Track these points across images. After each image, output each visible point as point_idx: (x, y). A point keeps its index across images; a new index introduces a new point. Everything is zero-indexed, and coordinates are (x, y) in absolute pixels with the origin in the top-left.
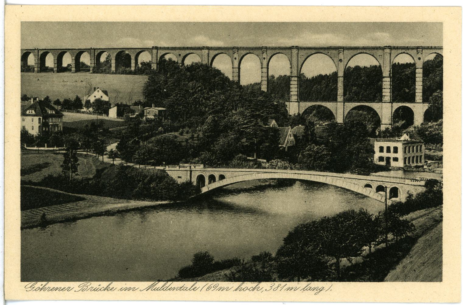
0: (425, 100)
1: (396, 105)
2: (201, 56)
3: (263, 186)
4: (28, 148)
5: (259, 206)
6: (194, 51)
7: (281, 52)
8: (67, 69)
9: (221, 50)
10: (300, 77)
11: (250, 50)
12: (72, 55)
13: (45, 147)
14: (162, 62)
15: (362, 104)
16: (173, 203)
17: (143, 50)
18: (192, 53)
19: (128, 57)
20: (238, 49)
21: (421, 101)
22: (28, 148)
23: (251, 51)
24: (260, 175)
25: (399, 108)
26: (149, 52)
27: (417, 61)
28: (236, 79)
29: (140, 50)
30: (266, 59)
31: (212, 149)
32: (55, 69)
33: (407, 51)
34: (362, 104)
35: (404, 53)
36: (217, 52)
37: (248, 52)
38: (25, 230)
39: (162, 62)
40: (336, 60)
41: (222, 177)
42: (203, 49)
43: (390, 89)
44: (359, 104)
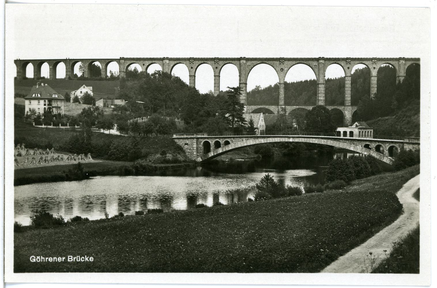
0: (353, 104)
2: (163, 65)
4: (35, 126)
6: (156, 62)
9: (179, 61)
10: (286, 84)
11: (204, 61)
13: (67, 126)
15: (262, 107)
18: (154, 63)
21: (350, 104)
22: (35, 126)
23: (205, 62)
26: (117, 62)
28: (192, 85)
29: (109, 61)
30: (144, 63)
31: (249, 125)
34: (262, 107)
38: (362, 130)
40: (279, 69)
41: (227, 143)
42: (164, 60)
43: (318, 94)
44: (259, 107)
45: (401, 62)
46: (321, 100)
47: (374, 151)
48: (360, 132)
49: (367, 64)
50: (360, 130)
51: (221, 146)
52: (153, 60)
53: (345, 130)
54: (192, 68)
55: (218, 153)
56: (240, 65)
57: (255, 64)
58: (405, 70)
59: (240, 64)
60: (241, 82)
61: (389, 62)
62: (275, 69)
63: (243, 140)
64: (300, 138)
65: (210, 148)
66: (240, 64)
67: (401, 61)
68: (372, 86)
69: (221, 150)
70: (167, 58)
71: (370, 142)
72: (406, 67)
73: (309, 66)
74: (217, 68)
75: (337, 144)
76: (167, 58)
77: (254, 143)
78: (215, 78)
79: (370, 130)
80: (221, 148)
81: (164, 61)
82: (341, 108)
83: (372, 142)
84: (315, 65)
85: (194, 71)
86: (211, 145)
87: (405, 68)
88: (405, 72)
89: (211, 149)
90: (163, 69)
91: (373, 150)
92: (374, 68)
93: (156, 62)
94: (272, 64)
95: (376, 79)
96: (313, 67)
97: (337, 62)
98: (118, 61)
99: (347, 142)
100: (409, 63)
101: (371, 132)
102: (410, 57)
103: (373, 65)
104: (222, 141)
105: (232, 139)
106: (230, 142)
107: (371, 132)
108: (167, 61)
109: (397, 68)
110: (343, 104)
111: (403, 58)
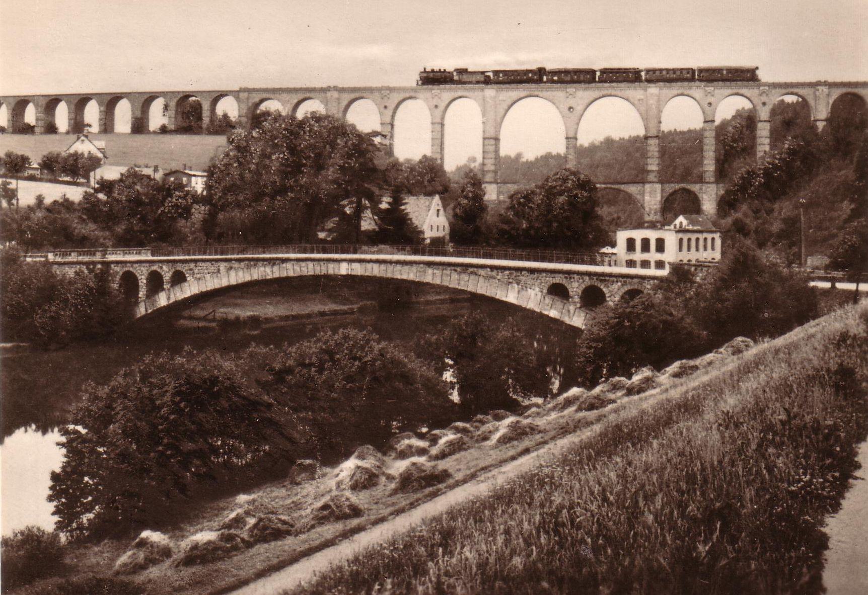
0: (721, 174)
1: (671, 188)
2: (326, 102)
3: (56, 246)
5: (841, 408)
6: (311, 95)
7: (686, 93)
8: (28, 130)
12: (100, 104)
14: (256, 119)
16: (448, 358)
17: (221, 95)
19: (198, 107)
20: (391, 90)
21: (712, 179)
24: (276, 268)
25: (675, 192)
27: (759, 107)
32: (11, 130)
33: (795, 90)
35: (682, 94)
36: (353, 96)
37: (407, 95)
39: (256, 119)
42: (329, 91)
45: (820, 90)
46: (653, 171)
47: (579, 305)
48: (681, 240)
49: (748, 95)
50: (680, 235)
51: (165, 287)
52: (306, 94)
53: (645, 237)
54: (386, 107)
55: (159, 307)
56: (484, 100)
57: (515, 98)
58: (830, 107)
59: (484, 99)
60: (487, 135)
61: (795, 90)
62: (558, 108)
63: (219, 271)
64: (367, 264)
65: (138, 294)
66: (484, 99)
67: (820, 88)
68: (759, 141)
69: (165, 299)
70: (334, 87)
71: (566, 278)
72: (831, 102)
73: (627, 100)
74: (436, 106)
75: (470, 281)
76: (336, 89)
77: (248, 278)
78: (433, 128)
79: (709, 236)
80: (164, 292)
81: (329, 94)
82: (695, 188)
83: (570, 278)
84: (639, 100)
85: (390, 113)
86: (140, 284)
87: (828, 103)
88: (829, 110)
89: (140, 295)
90: (327, 109)
91: (575, 302)
92: (764, 104)
93: (313, 97)
94: (551, 97)
95: (767, 126)
96: (636, 102)
97: (686, 92)
98: (236, 94)
99: (499, 277)
100: (836, 93)
101: (713, 239)
102: (838, 80)
103: (762, 98)
104: (167, 273)
105: (192, 265)
106: (187, 275)
107: (713, 239)
108: (335, 94)
109: (812, 102)
110: (701, 180)
111: (825, 82)
